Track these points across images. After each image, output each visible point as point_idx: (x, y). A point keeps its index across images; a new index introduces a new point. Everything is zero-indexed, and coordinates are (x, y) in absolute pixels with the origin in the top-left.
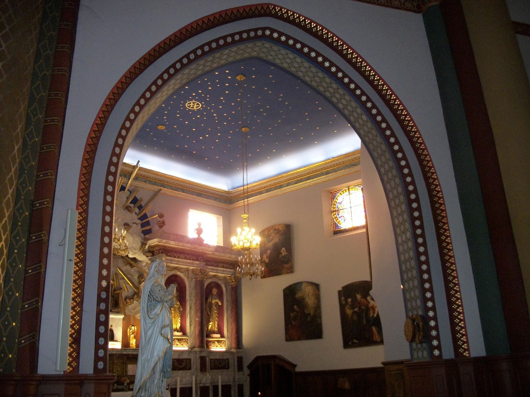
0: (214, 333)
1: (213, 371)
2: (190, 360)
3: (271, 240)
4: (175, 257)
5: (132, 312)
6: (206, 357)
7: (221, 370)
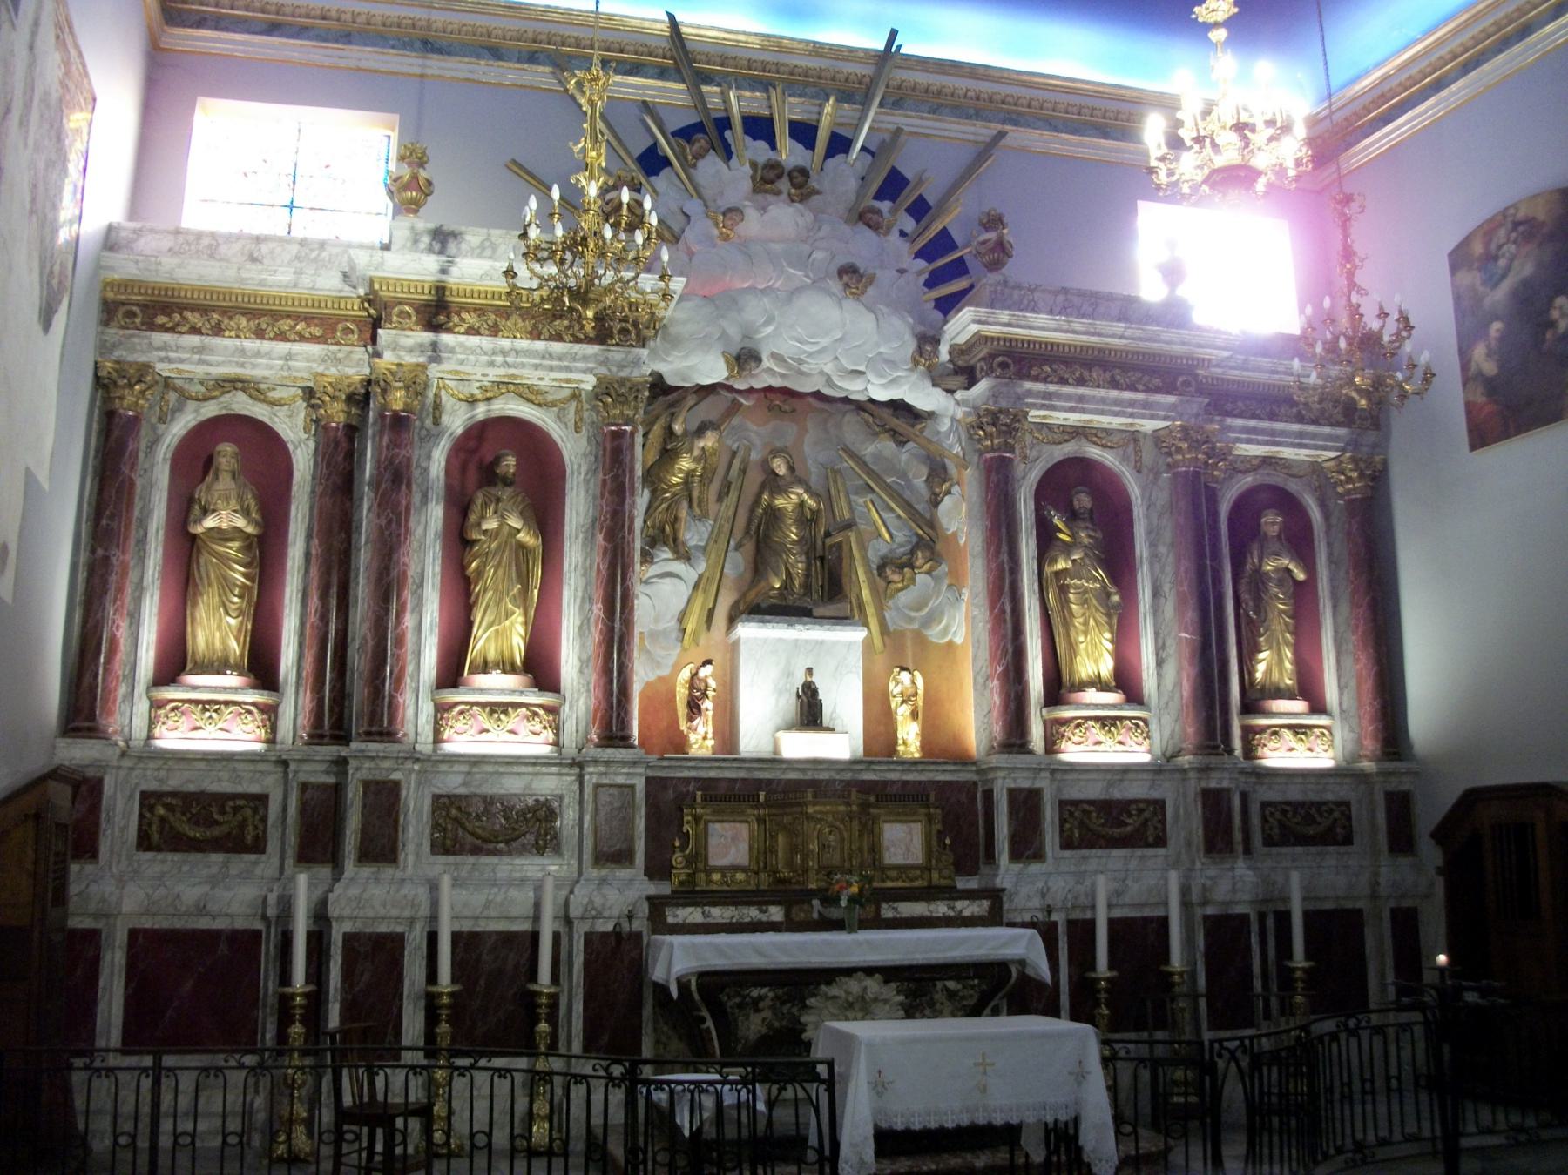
0: (1279, 693)
1: (1275, 850)
2: (1160, 805)
3: (1504, 276)
4: (1063, 381)
5: (911, 620)
6: (1228, 790)
7: (1313, 849)
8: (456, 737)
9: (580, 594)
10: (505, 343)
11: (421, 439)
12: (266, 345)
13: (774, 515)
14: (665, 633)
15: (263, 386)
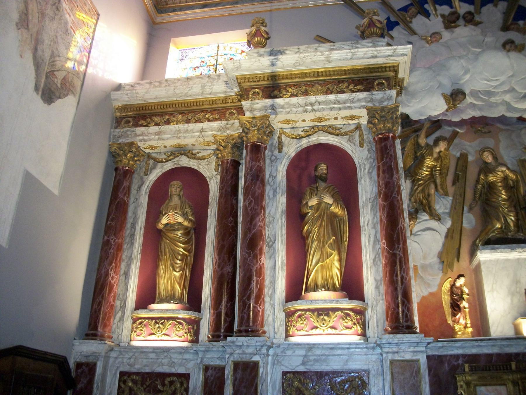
9: (372, 239)
10: (312, 98)
11: (272, 161)
12: (191, 126)
13: (491, 187)
14: (431, 266)
15: (194, 152)
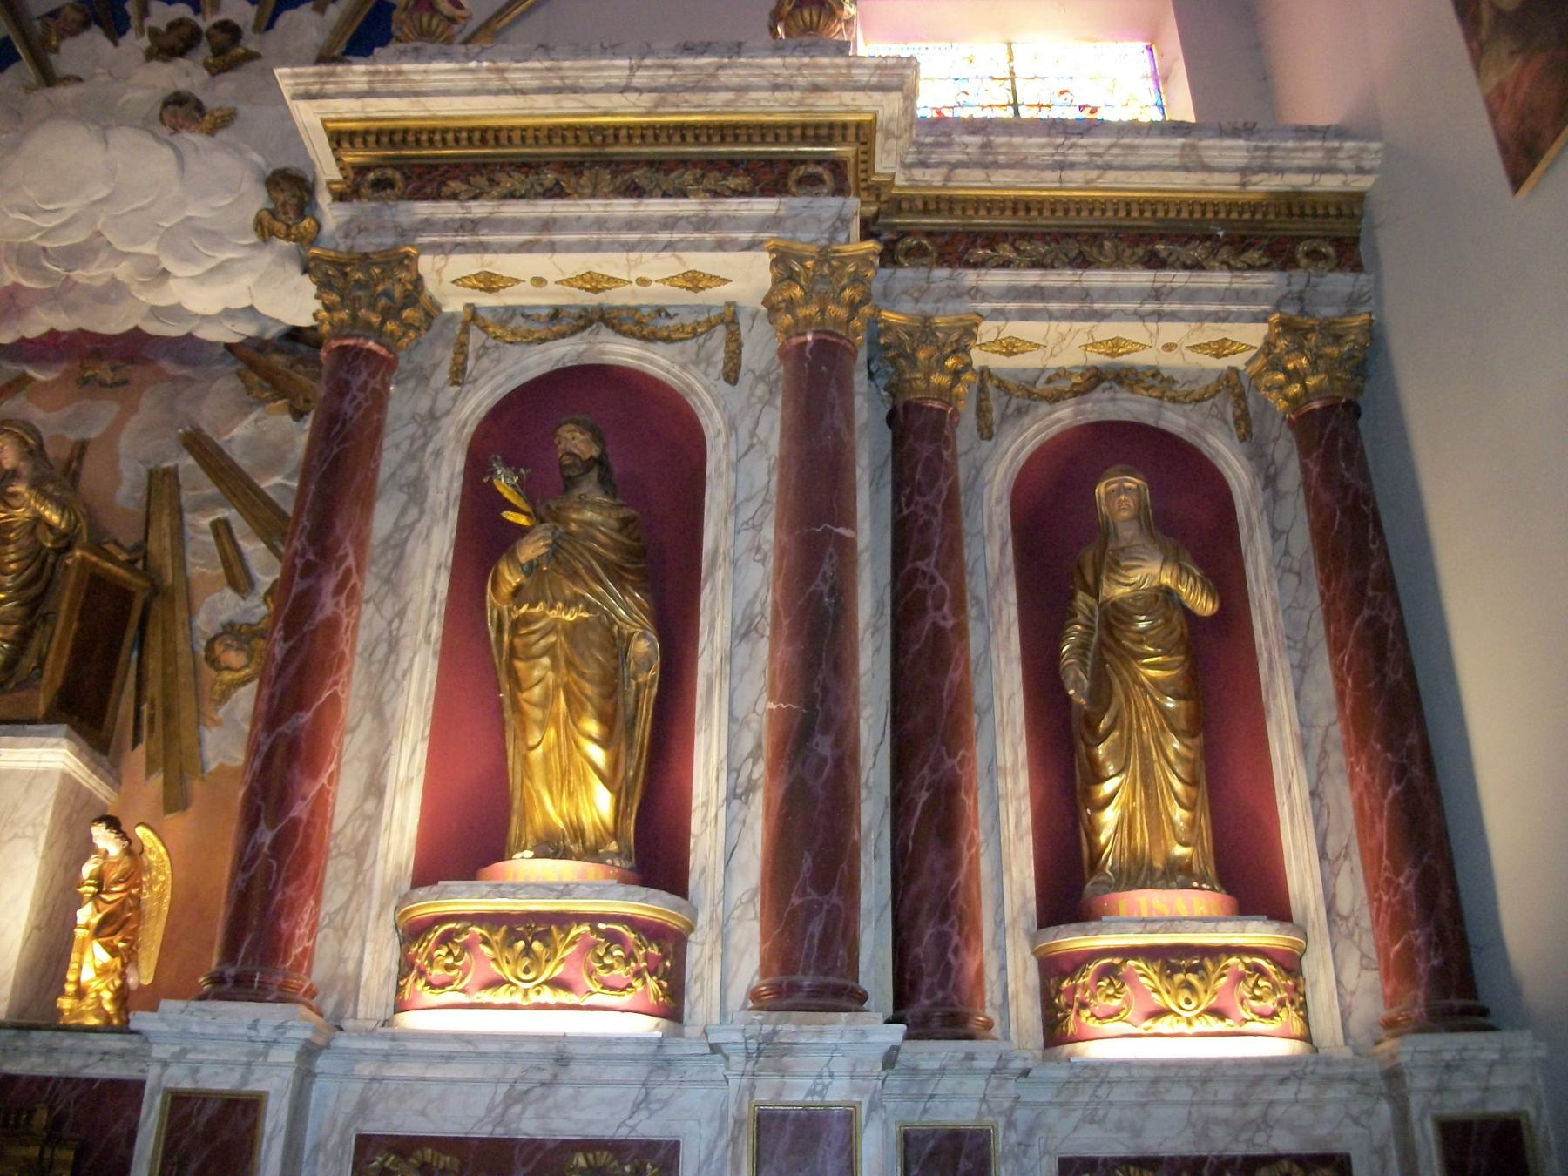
8: (430, 997)
